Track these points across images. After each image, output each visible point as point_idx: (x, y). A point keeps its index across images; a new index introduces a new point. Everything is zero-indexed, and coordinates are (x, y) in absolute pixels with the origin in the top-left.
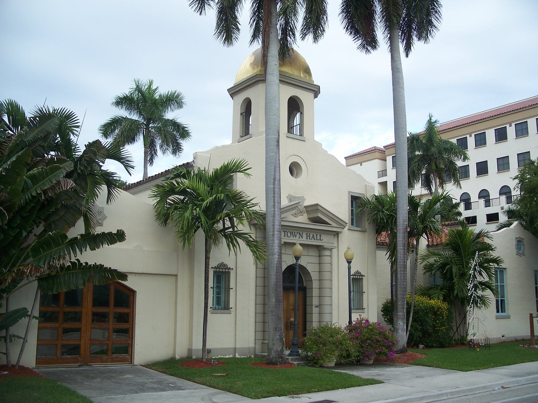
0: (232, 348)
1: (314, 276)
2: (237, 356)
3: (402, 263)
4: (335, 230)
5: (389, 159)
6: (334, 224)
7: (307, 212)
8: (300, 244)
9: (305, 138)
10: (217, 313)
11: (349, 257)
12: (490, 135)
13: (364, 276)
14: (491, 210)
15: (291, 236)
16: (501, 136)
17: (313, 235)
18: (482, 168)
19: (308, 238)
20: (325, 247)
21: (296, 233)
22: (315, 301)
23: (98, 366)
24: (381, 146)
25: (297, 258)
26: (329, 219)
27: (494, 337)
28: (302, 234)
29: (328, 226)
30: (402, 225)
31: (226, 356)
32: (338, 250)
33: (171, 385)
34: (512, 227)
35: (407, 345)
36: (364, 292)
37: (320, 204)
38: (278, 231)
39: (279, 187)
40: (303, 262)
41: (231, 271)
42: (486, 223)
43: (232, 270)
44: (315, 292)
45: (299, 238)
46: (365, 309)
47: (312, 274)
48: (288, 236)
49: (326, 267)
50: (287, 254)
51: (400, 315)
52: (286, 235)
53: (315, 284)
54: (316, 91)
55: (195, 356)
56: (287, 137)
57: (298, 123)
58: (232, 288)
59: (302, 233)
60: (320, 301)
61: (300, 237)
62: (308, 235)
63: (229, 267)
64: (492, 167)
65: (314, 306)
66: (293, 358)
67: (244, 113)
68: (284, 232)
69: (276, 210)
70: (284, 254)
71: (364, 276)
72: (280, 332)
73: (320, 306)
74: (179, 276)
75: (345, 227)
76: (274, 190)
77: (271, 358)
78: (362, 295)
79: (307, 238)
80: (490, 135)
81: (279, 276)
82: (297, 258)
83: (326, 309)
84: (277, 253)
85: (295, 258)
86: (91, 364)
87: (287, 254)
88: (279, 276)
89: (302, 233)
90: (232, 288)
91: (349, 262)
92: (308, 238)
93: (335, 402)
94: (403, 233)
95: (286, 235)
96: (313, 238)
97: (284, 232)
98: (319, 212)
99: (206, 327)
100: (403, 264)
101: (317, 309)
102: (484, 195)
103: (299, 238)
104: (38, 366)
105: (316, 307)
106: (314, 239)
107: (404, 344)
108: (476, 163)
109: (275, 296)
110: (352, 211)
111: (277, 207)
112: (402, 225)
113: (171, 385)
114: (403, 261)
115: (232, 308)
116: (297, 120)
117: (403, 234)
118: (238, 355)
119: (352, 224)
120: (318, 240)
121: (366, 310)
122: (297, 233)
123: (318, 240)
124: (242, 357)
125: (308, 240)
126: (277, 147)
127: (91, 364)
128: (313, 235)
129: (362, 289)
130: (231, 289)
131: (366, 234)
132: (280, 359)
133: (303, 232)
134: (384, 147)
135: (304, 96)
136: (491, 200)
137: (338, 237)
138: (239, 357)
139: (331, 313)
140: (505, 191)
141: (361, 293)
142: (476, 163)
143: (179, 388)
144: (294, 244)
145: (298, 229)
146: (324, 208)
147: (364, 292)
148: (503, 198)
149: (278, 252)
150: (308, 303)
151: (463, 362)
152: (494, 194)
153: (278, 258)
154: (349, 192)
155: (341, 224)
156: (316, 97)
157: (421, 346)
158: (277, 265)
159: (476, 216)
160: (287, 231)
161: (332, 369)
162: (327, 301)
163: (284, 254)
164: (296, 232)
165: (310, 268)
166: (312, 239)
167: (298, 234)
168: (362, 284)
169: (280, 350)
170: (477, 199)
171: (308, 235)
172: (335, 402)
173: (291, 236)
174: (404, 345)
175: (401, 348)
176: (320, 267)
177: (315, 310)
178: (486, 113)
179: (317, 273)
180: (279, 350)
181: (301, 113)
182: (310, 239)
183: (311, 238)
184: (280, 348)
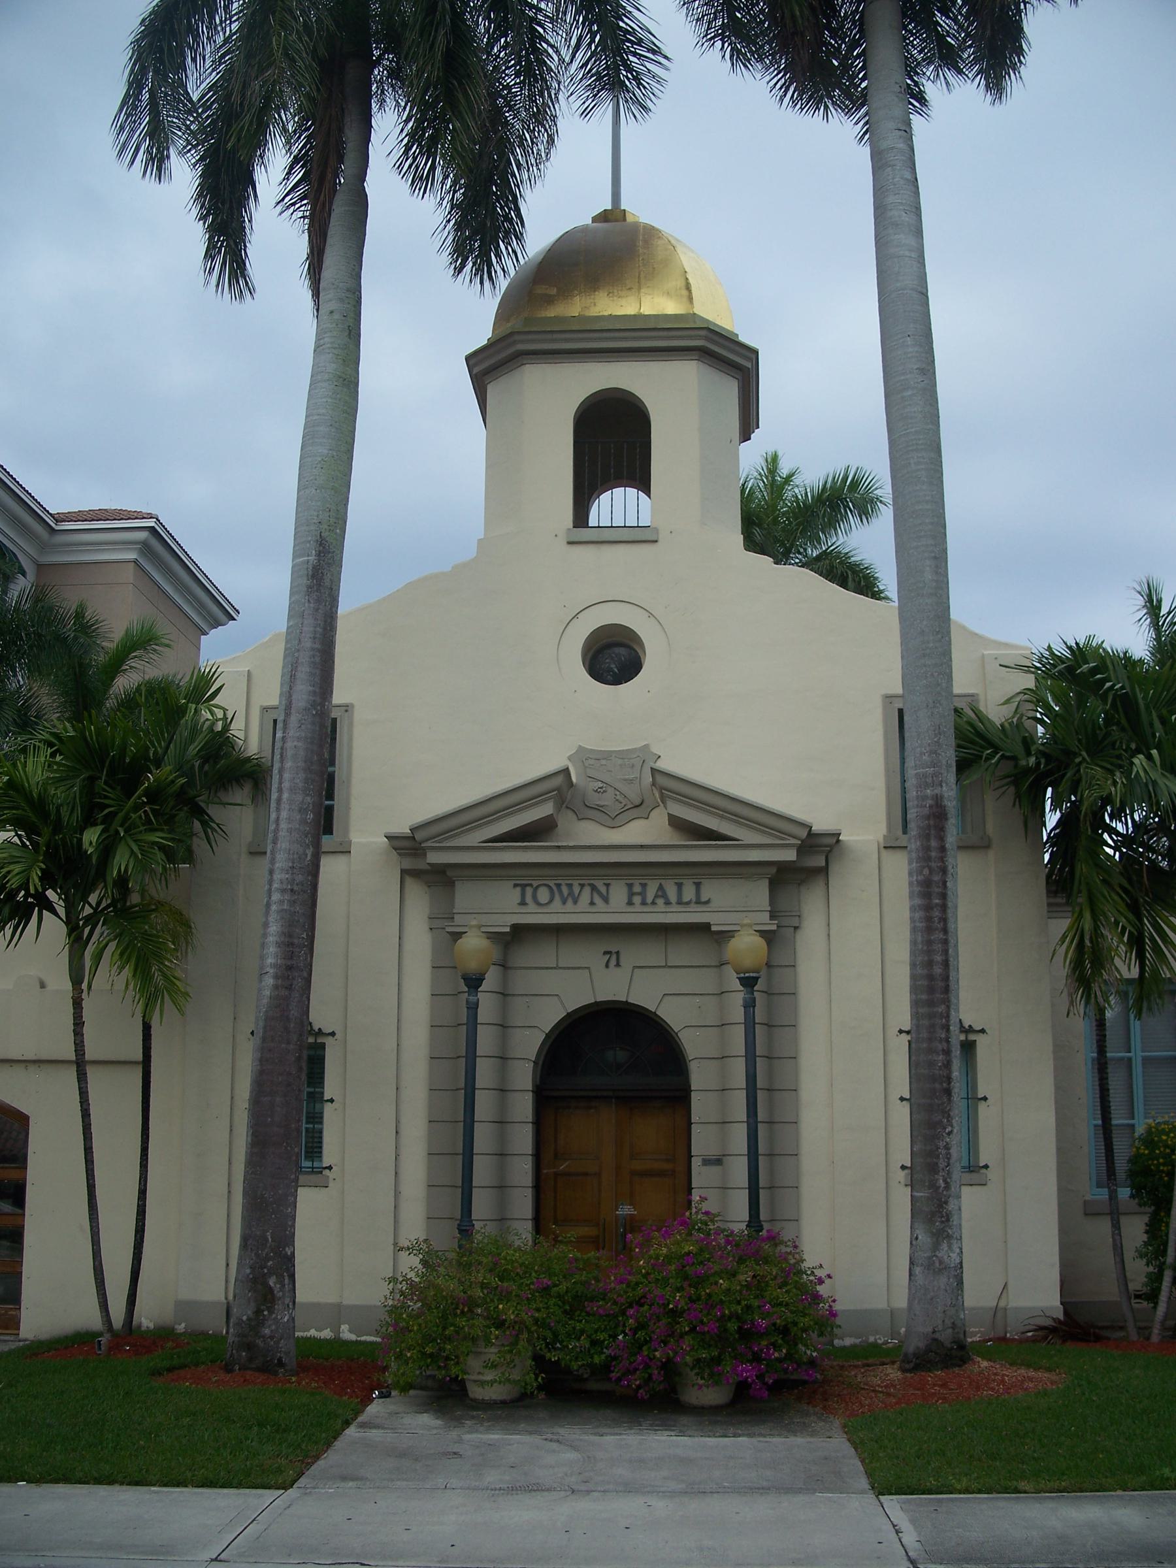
0: (991, 1308)
2: (347, 1334)
6: (747, 836)
10: (971, 1185)
13: (983, 1031)
17: (661, 888)
20: (714, 928)
21: (576, 889)
26: (722, 817)
27: (852, 1308)
28: (603, 890)
29: (726, 846)
30: (916, 802)
31: (308, 1331)
36: (985, 1099)
41: (980, 1040)
43: (331, 1037)
45: (592, 903)
46: (986, 1167)
50: (561, 968)
55: (183, 1325)
56: (569, 543)
58: (332, 1101)
59: (608, 885)
61: (597, 899)
62: (637, 889)
63: (316, 1028)
68: (518, 889)
69: (281, 817)
70: (551, 968)
71: (983, 1031)
72: (257, 1255)
79: (630, 903)
81: (270, 1050)
85: (464, 979)
87: (561, 968)
88: (270, 1050)
89: (608, 885)
90: (332, 1101)
92: (637, 900)
95: (529, 899)
96: (660, 901)
97: (518, 889)
98: (670, 797)
100: (925, 971)
103: (592, 903)
105: (706, 1162)
106: (668, 903)
107: (934, 1332)
111: (287, 807)
112: (916, 802)
114: (926, 958)
115: (330, 1168)
118: (350, 1331)
120: (688, 903)
121: (991, 1174)
122: (582, 886)
123: (688, 903)
124: (363, 1338)
125: (638, 908)
128: (661, 888)
130: (329, 1103)
131: (991, 854)
132: (244, 1354)
133: (608, 882)
137: (827, 884)
138: (353, 1337)
145: (536, 872)
146: (526, 785)
147: (985, 1099)
157: (211, 1332)
158: (266, 1011)
160: (531, 885)
163: (551, 968)
164: (576, 884)
167: (587, 890)
169: (249, 1319)
171: (637, 889)
174: (937, 1336)
175: (922, 1345)
180: (245, 1318)
182: (644, 903)
184: (249, 1312)
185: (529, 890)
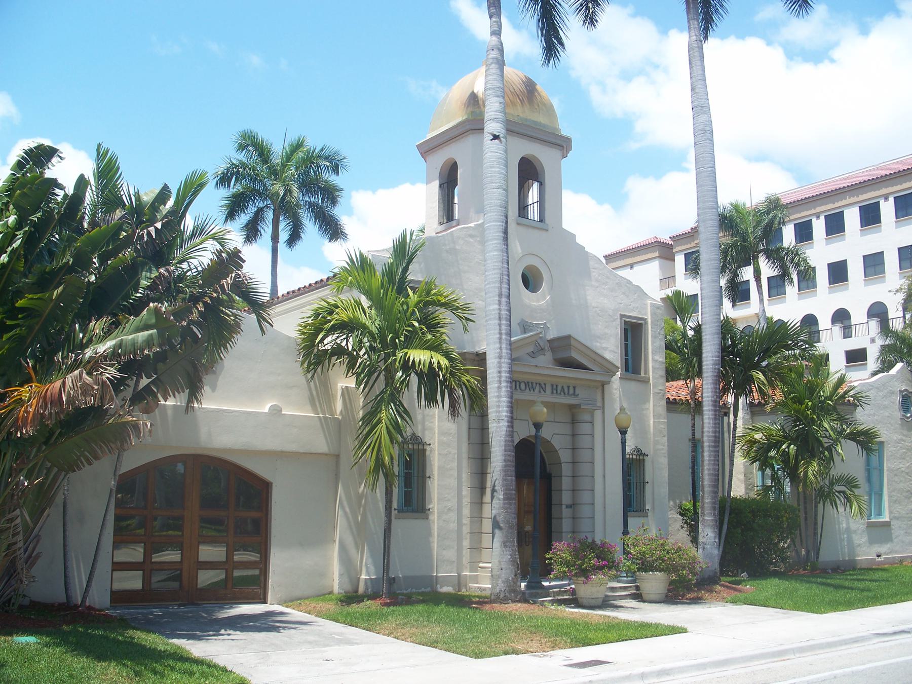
1: (565, 456)
3: (711, 434)
4: (599, 378)
5: (680, 260)
7: (552, 349)
8: (543, 403)
9: (547, 224)
11: (624, 424)
12: (852, 217)
14: (853, 344)
15: (526, 387)
16: (871, 216)
18: (838, 273)
19: (555, 392)
21: (534, 385)
22: (566, 498)
23: (211, 605)
24: (665, 238)
25: (538, 426)
28: (543, 386)
32: (603, 413)
33: (336, 637)
34: (893, 371)
35: (721, 570)
36: (648, 482)
37: (573, 335)
38: (507, 382)
39: (509, 308)
40: (545, 433)
42: (846, 366)
44: (566, 483)
45: (540, 392)
47: (561, 453)
48: (520, 389)
49: (584, 442)
51: (708, 520)
52: (518, 388)
53: (566, 470)
54: (563, 145)
57: (535, 200)
60: (574, 497)
61: (542, 390)
64: (855, 270)
65: (564, 507)
66: (532, 593)
67: (446, 185)
71: (647, 455)
73: (573, 506)
74: (341, 456)
75: (614, 374)
76: (499, 314)
77: (498, 592)
78: (644, 488)
80: (852, 217)
82: (538, 426)
83: (585, 511)
84: (506, 419)
86: (199, 602)
91: (623, 432)
92: (555, 392)
93: (609, 663)
94: (713, 383)
95: (518, 388)
96: (562, 393)
99: (389, 542)
101: (570, 510)
102: (841, 317)
103: (540, 392)
104: (115, 605)
105: (567, 507)
106: (564, 393)
108: (864, 257)
109: (503, 489)
110: (626, 346)
113: (336, 637)
116: (533, 194)
117: (712, 386)
119: (627, 370)
126: (504, 241)
127: (199, 602)
129: (644, 479)
134: (670, 238)
135: (543, 155)
136: (853, 327)
139: (593, 518)
140: (878, 312)
141: (642, 484)
142: (864, 257)
143: (349, 642)
144: (533, 403)
148: (874, 325)
149: (508, 416)
150: (554, 500)
151: (554, 612)
152: (858, 316)
153: (508, 426)
154: (622, 316)
155: (610, 370)
156: (564, 156)
159: (866, 348)
161: (11, 635)
162: (585, 497)
165: (557, 443)
166: (560, 394)
167: (538, 385)
168: (644, 470)
170: (829, 325)
172: (609, 663)
173: (526, 389)
176: (573, 442)
177: (566, 512)
178: (844, 178)
179: (570, 451)
180: (510, 579)
181: (541, 185)
183: (559, 392)
184: (513, 576)
185: (518, 383)
